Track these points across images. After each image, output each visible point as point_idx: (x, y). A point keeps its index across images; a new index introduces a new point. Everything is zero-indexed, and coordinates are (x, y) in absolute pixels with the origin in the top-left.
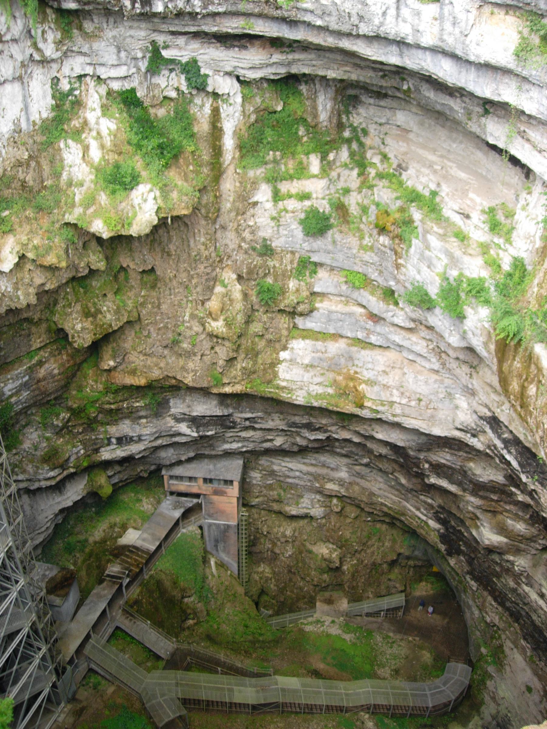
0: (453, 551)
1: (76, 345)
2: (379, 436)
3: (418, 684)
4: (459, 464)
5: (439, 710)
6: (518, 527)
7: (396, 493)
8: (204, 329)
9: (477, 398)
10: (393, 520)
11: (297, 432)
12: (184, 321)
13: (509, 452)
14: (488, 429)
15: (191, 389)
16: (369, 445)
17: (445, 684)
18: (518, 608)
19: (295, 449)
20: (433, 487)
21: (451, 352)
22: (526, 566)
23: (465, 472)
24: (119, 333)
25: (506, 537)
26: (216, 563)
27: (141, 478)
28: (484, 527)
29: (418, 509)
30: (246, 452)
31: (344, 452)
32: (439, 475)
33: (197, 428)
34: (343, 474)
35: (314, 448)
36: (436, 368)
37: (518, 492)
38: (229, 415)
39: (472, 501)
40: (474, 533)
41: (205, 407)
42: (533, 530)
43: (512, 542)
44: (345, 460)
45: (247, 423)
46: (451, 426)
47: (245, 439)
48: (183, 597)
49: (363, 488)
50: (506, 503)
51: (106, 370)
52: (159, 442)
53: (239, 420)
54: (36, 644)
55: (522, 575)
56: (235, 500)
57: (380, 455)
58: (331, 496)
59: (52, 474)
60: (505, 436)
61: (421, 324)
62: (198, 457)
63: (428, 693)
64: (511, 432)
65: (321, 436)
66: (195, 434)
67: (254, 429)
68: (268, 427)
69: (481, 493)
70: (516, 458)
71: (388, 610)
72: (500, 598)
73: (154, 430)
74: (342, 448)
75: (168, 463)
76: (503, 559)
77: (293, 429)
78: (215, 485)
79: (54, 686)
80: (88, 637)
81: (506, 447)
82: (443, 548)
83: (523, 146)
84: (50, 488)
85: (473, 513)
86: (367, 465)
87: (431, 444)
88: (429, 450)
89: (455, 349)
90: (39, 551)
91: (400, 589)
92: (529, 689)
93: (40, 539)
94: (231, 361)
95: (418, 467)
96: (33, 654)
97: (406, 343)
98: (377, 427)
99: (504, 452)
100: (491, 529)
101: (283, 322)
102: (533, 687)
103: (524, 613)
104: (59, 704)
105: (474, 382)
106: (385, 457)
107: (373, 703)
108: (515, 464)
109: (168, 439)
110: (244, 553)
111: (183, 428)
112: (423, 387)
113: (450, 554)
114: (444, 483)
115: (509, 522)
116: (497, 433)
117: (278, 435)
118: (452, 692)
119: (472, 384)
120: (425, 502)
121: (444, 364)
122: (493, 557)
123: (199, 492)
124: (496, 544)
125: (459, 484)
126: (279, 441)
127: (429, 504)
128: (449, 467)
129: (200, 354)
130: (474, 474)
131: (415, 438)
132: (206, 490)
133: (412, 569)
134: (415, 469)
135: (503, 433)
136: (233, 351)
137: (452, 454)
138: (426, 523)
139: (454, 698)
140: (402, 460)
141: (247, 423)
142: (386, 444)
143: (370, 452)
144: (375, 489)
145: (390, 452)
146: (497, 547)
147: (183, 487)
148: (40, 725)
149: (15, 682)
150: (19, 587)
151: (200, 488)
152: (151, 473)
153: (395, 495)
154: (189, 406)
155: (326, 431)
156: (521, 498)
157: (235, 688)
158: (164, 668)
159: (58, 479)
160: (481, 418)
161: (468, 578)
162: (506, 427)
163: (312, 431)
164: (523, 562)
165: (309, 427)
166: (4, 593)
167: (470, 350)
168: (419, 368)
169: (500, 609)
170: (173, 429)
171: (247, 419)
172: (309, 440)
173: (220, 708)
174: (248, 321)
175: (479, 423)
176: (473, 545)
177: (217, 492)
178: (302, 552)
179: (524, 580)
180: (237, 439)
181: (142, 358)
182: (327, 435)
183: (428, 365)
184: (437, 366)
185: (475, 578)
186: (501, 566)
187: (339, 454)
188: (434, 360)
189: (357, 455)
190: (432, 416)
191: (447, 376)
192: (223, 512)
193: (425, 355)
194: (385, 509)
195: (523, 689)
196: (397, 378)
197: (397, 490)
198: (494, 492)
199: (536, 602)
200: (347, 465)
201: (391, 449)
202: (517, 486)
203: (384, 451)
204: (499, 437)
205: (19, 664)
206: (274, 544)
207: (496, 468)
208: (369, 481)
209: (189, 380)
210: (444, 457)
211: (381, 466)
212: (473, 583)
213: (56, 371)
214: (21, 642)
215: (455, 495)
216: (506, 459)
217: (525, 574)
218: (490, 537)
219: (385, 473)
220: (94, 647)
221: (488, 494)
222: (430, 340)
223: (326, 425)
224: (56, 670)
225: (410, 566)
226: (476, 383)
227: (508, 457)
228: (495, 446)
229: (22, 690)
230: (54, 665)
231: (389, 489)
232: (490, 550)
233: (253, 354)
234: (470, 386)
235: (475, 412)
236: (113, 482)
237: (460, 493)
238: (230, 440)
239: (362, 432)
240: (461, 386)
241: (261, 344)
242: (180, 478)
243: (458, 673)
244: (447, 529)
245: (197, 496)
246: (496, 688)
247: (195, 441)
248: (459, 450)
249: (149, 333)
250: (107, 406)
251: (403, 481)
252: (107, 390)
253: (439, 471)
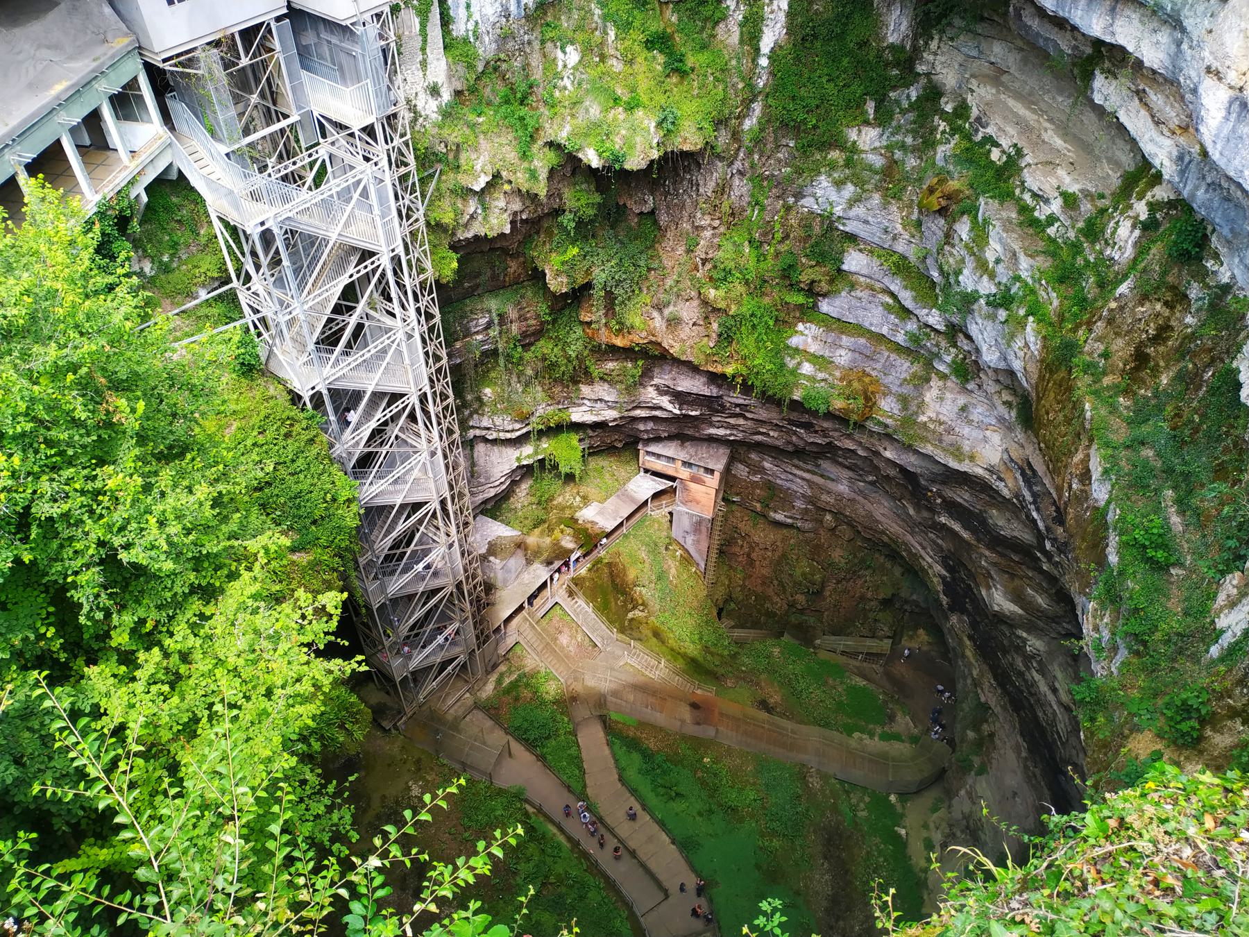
0: (957, 606)
10: (892, 551)
15: (676, 362)
19: (790, 448)
22: (1042, 649)
25: (1021, 608)
32: (951, 516)
33: (680, 405)
34: (843, 488)
37: (1044, 560)
38: (721, 397)
39: (986, 558)
40: (984, 593)
42: (1057, 608)
47: (733, 427)
50: (1028, 568)
66: (677, 412)
67: (746, 418)
72: (1002, 678)
74: (846, 458)
82: (944, 600)
83: (1138, 112)
86: (872, 483)
106: (893, 478)
111: (665, 401)
113: (952, 608)
114: (956, 527)
120: (934, 542)
125: (974, 531)
137: (971, 494)
143: (877, 468)
145: (899, 476)
147: (659, 465)
159: (518, 433)
165: (808, 426)
167: (1011, 373)
171: (737, 405)
177: (695, 479)
182: (828, 440)
187: (840, 464)
197: (903, 520)
198: (1016, 552)
203: (892, 472)
209: (675, 351)
219: (894, 498)
221: (1008, 552)
229: (433, 653)
232: (1000, 618)
242: (659, 456)
245: (673, 479)
248: (982, 491)
251: (911, 512)
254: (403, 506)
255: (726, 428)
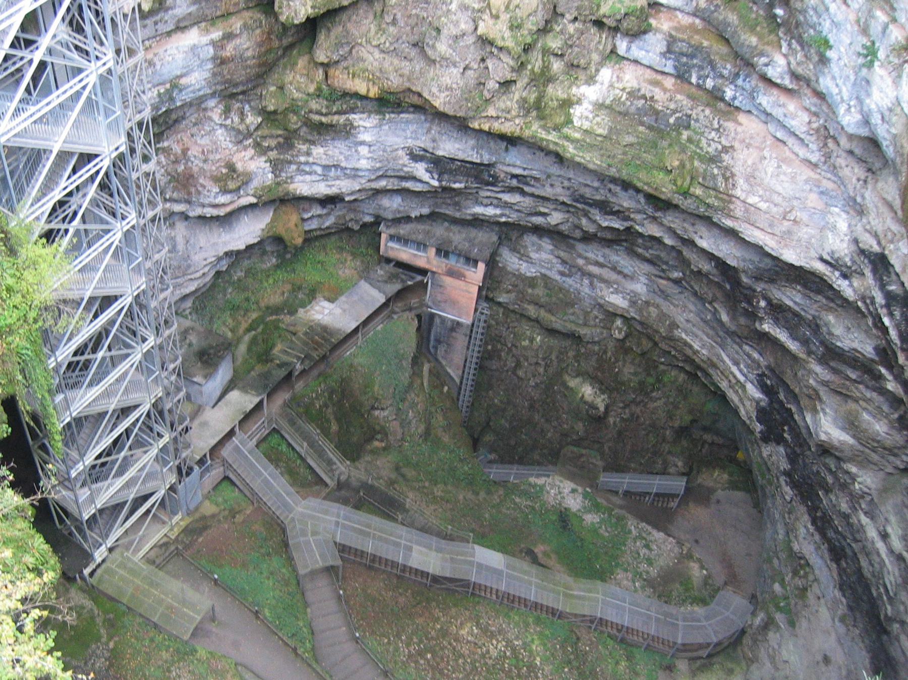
0: (772, 435)
1: (283, 18)
2: (703, 244)
3: (672, 609)
4: (812, 312)
5: (690, 651)
6: (878, 428)
7: (711, 332)
8: (476, 29)
9: (864, 220)
11: (583, 210)
12: (449, 11)
13: (891, 315)
14: (868, 272)
16: (687, 253)
17: (707, 618)
18: (844, 543)
20: (765, 337)
21: (843, 141)
22: (873, 486)
23: (817, 326)
24: (349, 12)
25: (854, 437)
26: (430, 371)
27: (348, 229)
28: (825, 413)
29: (737, 364)
30: (505, 223)
31: (647, 255)
32: (776, 321)
35: (604, 239)
36: (814, 160)
37: (890, 377)
40: (809, 419)
41: (457, 146)
43: (860, 448)
44: (647, 268)
45: (514, 182)
46: (814, 254)
47: (507, 205)
48: (373, 408)
49: (664, 315)
50: (867, 387)
51: (322, 64)
52: (383, 183)
53: (502, 175)
54: (157, 428)
55: (863, 497)
56: (475, 290)
57: (699, 272)
58: (615, 315)
59: (222, 199)
60: (892, 288)
61: (808, 85)
62: (433, 216)
63: (680, 623)
64: (903, 284)
65: (617, 224)
67: (523, 193)
68: (543, 194)
69: (832, 364)
70: (897, 326)
71: (657, 495)
72: (821, 522)
73: (378, 165)
74: (646, 249)
75: (390, 217)
76: (841, 468)
77: (579, 205)
78: (452, 261)
79: (172, 488)
80: (231, 434)
81: (888, 306)
82: (758, 427)
84: (217, 218)
85: (814, 390)
86: (677, 282)
87: (777, 273)
88: (772, 281)
89: (851, 137)
90: (189, 304)
91: (683, 470)
92: (826, 660)
93: (192, 287)
94: (506, 85)
95: (750, 302)
96: (152, 442)
97: (777, 112)
98: (702, 229)
99: (883, 312)
100: (835, 420)
101: (597, 40)
102: (833, 659)
103: (848, 551)
104: (175, 513)
105: (868, 194)
106: (706, 275)
107: (599, 615)
108: (893, 334)
109: (396, 181)
110: (473, 366)
111: (420, 170)
112: (786, 185)
113: (766, 439)
114: (782, 336)
115: (866, 416)
116: (881, 280)
117: (556, 209)
118: (715, 632)
119: (863, 197)
120: (749, 356)
121: (828, 156)
122: (827, 461)
123: (427, 266)
124: (836, 443)
125: (805, 342)
126: (556, 218)
127: (754, 361)
128: (796, 314)
129: (462, 66)
130: (830, 334)
131: (756, 259)
132: (438, 267)
133: (707, 446)
134: (744, 305)
135: (888, 284)
136: (513, 70)
137: (805, 296)
138: (743, 387)
139: (715, 640)
140: (728, 287)
141: (514, 182)
142: (711, 257)
143: (686, 263)
144: (680, 319)
145: (715, 271)
146: (837, 449)
147: (405, 254)
148: (144, 536)
149: (121, 472)
150: (146, 347)
151: (429, 262)
152: (364, 225)
153: (708, 335)
154: (434, 141)
155: (627, 219)
156: (891, 385)
157: (415, 547)
158: (324, 499)
160: (862, 252)
161: (782, 479)
162: (897, 275)
163: (607, 213)
164: (869, 481)
165: (604, 207)
166: (125, 351)
168: (788, 153)
169: (817, 537)
170: (405, 169)
171: (514, 176)
172: (600, 225)
173: (389, 569)
174: (545, 30)
175: (856, 258)
176: (801, 445)
177: (451, 273)
178: (553, 385)
179: (863, 506)
180: (495, 202)
181: (377, 54)
182: (627, 224)
183: (802, 152)
184: (815, 158)
185: (794, 485)
186: (837, 478)
188: (813, 147)
189: (667, 263)
190: (789, 232)
191: (829, 175)
192: (454, 303)
193: (802, 136)
194: (689, 352)
195: (819, 658)
196: (750, 162)
197: (713, 328)
198: (854, 368)
199: (873, 542)
200: (648, 275)
201: (716, 267)
202: (890, 368)
203: (706, 266)
204: (882, 287)
205: (130, 448)
206: (518, 365)
207: (866, 332)
208: (676, 306)
210: (791, 297)
211: (697, 288)
212: (787, 489)
213: (249, 53)
214: (137, 420)
215: (795, 357)
216: (883, 323)
217: (868, 498)
218: (830, 431)
220: (237, 449)
222: (816, 114)
223: (628, 209)
224: (179, 469)
225: (705, 442)
226: (869, 197)
227: (886, 321)
228: (873, 299)
229: (128, 485)
230: (177, 463)
231: (702, 324)
232: (826, 450)
233: (544, 78)
234: (859, 199)
235: (856, 241)
236: (307, 228)
237: (803, 356)
238: (485, 201)
239: (679, 232)
240: (845, 195)
241: (557, 66)
243: (733, 607)
244: (771, 402)
245: (423, 272)
246: (780, 646)
247: (432, 194)
248: (819, 292)
249: (394, 19)
250: (316, 118)
251: (725, 318)
252: (319, 93)
253: (780, 316)
254: (64, 156)
255: (496, 206)
